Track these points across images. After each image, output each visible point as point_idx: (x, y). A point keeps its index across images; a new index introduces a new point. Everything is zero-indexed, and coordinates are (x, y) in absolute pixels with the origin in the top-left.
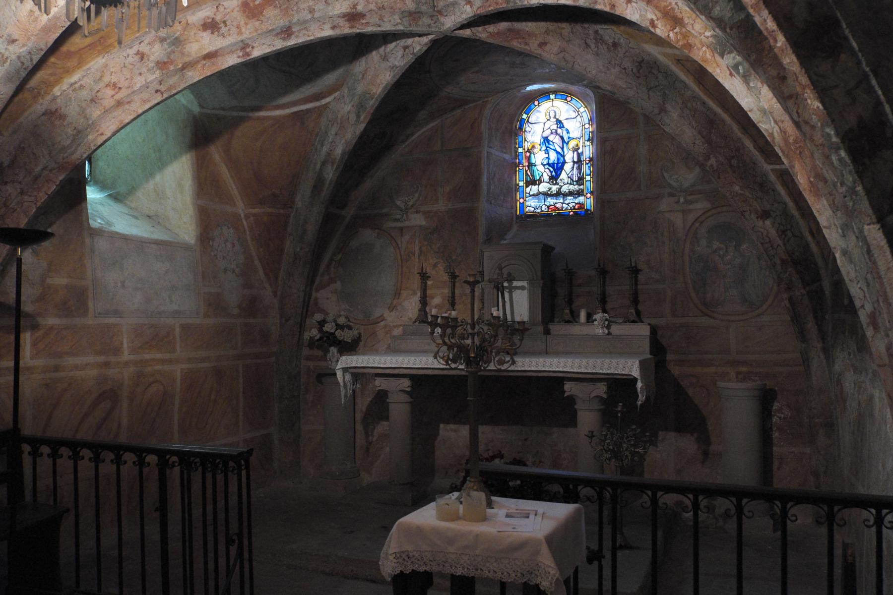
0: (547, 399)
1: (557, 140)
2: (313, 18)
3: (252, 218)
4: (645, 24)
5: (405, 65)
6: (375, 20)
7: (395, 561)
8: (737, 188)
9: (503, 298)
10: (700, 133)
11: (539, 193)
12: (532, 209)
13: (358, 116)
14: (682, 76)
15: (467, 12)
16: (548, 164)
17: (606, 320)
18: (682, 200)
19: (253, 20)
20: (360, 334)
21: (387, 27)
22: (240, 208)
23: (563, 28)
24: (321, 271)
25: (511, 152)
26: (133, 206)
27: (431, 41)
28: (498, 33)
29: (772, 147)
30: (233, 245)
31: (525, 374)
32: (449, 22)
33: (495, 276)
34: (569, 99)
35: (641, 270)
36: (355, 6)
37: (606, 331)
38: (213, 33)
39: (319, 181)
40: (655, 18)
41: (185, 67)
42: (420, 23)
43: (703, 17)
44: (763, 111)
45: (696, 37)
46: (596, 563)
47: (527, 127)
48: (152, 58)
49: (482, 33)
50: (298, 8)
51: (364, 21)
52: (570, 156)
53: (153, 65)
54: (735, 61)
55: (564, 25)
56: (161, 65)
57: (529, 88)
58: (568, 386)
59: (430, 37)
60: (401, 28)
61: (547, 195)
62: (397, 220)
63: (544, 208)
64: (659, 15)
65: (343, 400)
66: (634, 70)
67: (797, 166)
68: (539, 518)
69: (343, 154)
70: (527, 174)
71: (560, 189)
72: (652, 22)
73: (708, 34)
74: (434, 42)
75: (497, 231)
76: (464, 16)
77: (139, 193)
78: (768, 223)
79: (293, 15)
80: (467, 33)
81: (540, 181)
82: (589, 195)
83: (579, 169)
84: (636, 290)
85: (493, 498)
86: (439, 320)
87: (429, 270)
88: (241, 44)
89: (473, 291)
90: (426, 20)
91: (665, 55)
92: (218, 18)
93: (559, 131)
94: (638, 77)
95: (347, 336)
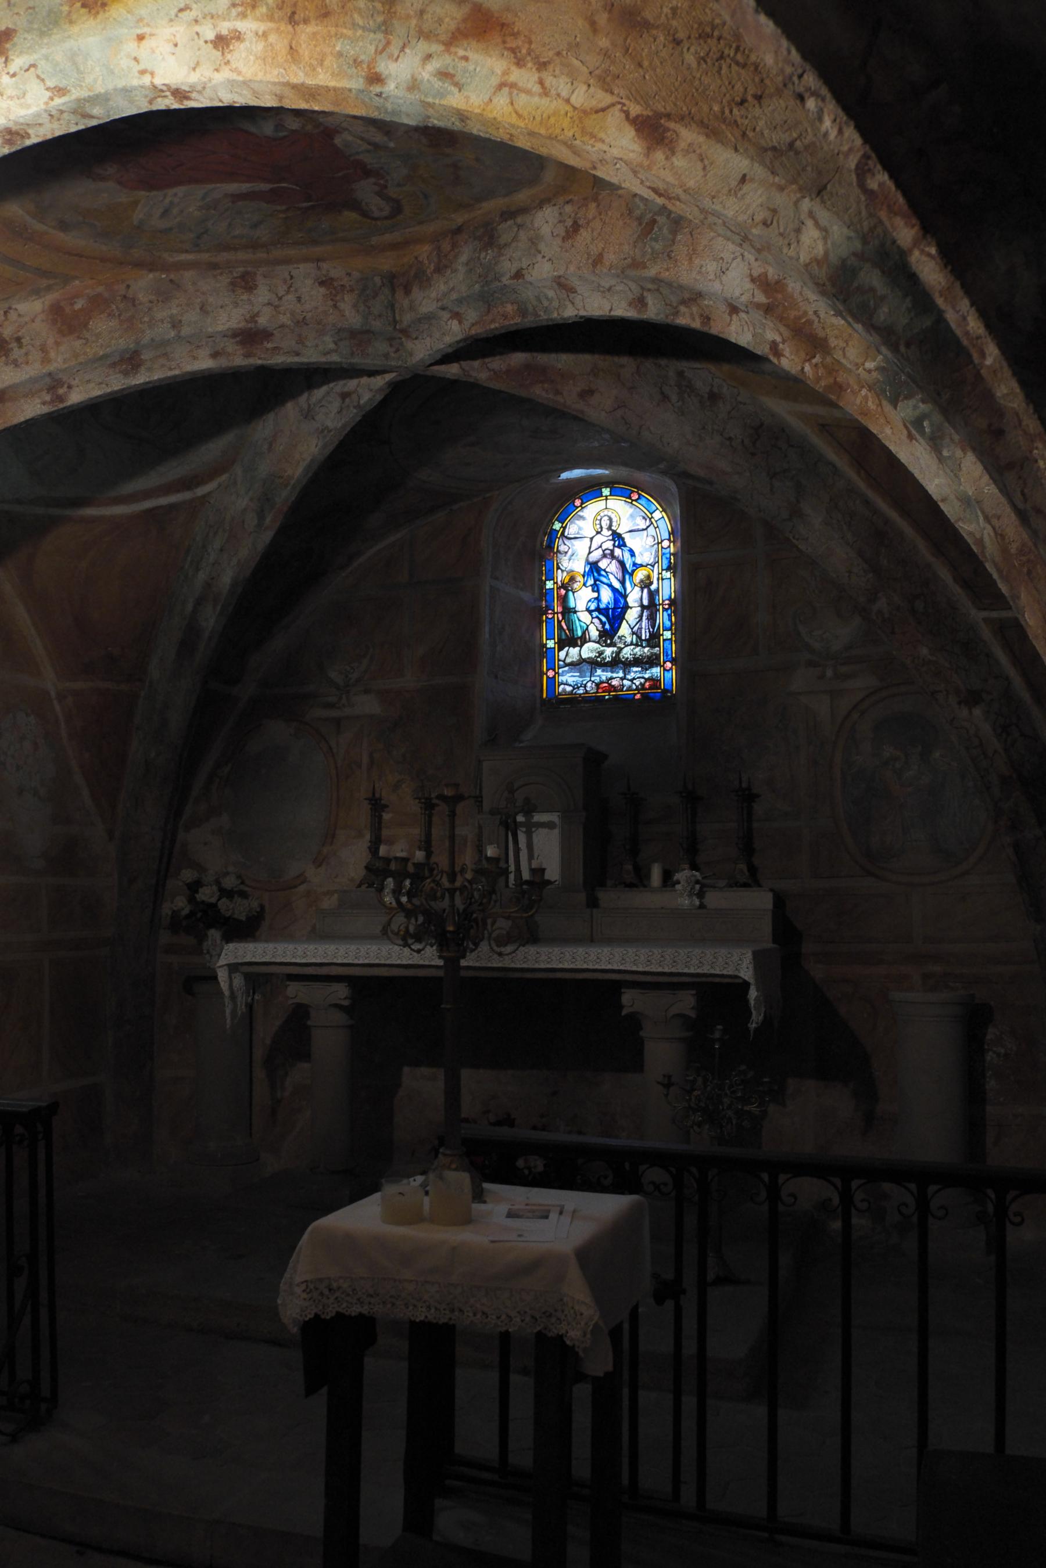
0: (589, 1019)
1: (613, 567)
2: (179, 337)
4: (762, 350)
7: (305, 1295)
8: (924, 651)
9: (516, 842)
11: (582, 661)
12: (569, 689)
13: (261, 515)
15: (454, 332)
17: (697, 882)
18: (829, 673)
20: (262, 907)
21: (311, 356)
23: (622, 366)
27: (390, 384)
29: (981, 564)
31: (551, 975)
32: (421, 350)
34: (635, 496)
35: (758, 796)
36: (253, 318)
37: (697, 902)
40: (778, 339)
43: (859, 327)
44: (966, 501)
45: (850, 371)
46: (670, 1304)
49: (479, 371)
51: (270, 345)
52: (635, 596)
54: (917, 413)
55: (624, 360)
57: (565, 475)
58: (628, 997)
59: (389, 377)
60: (335, 358)
61: (594, 664)
64: (787, 333)
65: (228, 1021)
67: (1025, 598)
68: (566, 1219)
72: (774, 346)
73: (870, 365)
74: (396, 389)
76: (448, 339)
78: (977, 712)
79: (143, 332)
80: (453, 370)
81: (584, 640)
82: (669, 665)
83: (652, 619)
85: (485, 1185)
86: (393, 866)
88: (48, 380)
89: (453, 814)
90: (381, 347)
93: (618, 552)
94: (753, 454)
95: (239, 909)
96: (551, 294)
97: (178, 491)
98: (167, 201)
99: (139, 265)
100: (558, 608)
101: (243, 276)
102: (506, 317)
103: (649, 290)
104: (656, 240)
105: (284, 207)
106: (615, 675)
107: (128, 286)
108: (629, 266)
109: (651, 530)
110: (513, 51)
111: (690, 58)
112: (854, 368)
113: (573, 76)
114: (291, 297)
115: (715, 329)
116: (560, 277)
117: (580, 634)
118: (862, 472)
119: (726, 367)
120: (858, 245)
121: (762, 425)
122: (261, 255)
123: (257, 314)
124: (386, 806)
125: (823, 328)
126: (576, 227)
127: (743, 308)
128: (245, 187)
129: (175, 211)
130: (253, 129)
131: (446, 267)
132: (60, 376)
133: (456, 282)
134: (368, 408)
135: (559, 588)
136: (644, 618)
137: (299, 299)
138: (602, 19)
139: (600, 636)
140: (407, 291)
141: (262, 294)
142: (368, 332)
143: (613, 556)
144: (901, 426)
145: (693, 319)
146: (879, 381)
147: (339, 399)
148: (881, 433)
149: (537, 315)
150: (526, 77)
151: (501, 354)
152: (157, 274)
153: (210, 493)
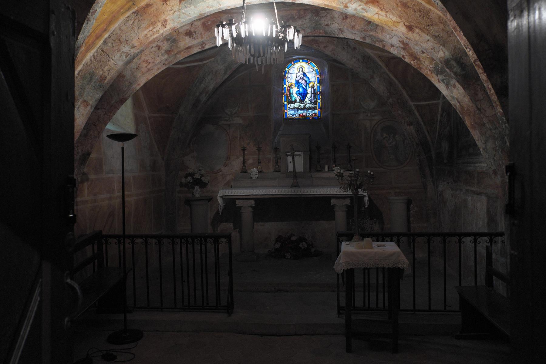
1: (303, 82)
8: (400, 112)
11: (294, 108)
18: (369, 115)
40: (405, 54)
48: (164, 48)
52: (309, 90)
53: (164, 52)
56: (168, 52)
58: (333, 201)
61: (298, 109)
62: (227, 121)
78: (412, 127)
92: (192, 30)
93: (304, 78)
110: (380, 7)
111: (418, 15)
113: (393, 14)
120: (451, 57)
138: (399, 4)
143: (303, 79)
150: (383, 13)
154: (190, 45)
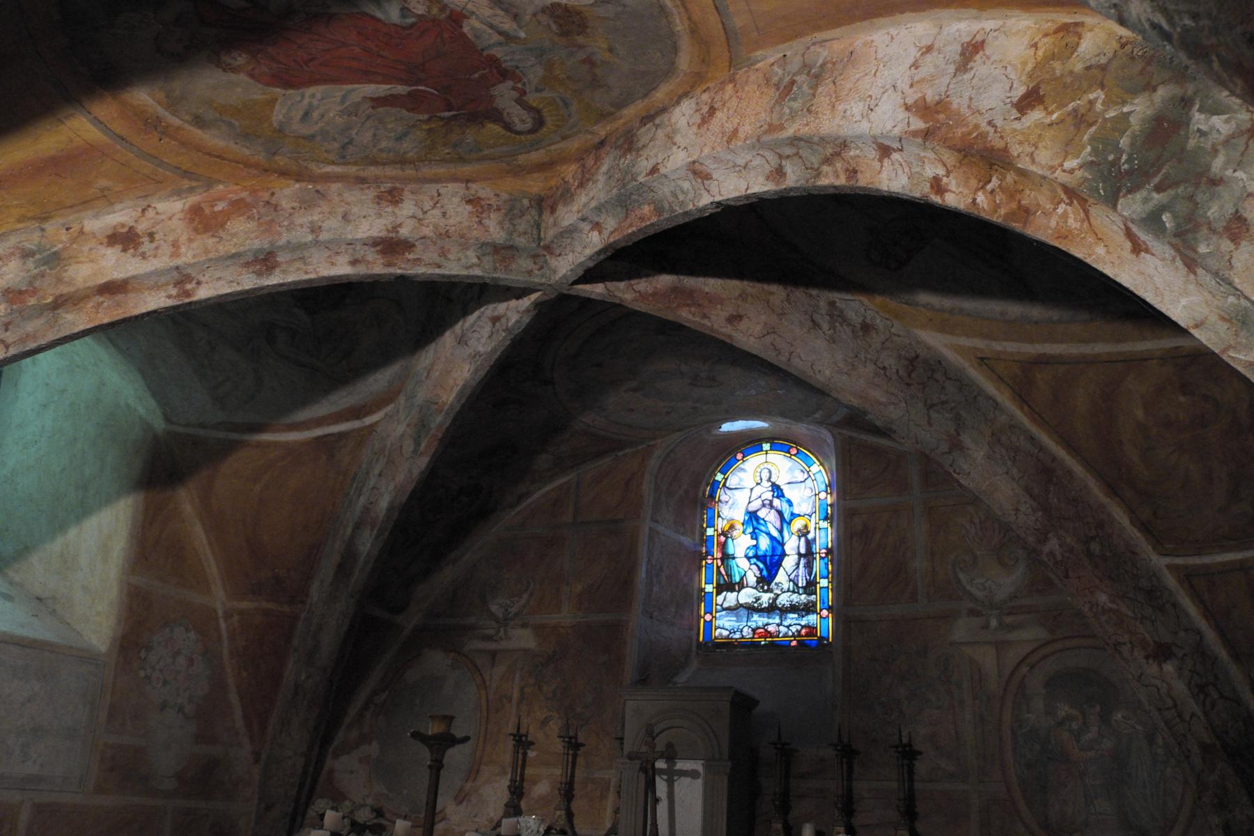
3: (236, 618)
5: (494, 350)
6: (432, 255)
8: (1103, 598)
10: (1028, 490)
11: (739, 606)
12: (725, 633)
13: (417, 443)
14: (990, 388)
15: (592, 243)
16: (756, 556)
18: (994, 623)
19: (205, 236)
22: (219, 598)
23: (772, 293)
24: (347, 720)
25: (693, 533)
26: (17, 579)
27: (537, 304)
28: (654, 294)
30: (191, 661)
33: (644, 749)
34: (794, 451)
35: (920, 753)
36: (395, 228)
38: (124, 250)
39: (349, 555)
40: (941, 171)
41: (59, 303)
42: (514, 266)
47: (722, 495)
50: (292, 223)
51: (411, 256)
52: (792, 545)
54: (1150, 206)
55: (774, 288)
57: (727, 427)
60: (477, 272)
61: (751, 609)
62: (489, 638)
63: (747, 632)
64: (950, 158)
66: (901, 372)
69: (390, 509)
70: (719, 573)
71: (775, 600)
75: (658, 669)
76: (588, 252)
77: (34, 559)
78: (1169, 667)
79: (280, 234)
81: (741, 585)
82: (825, 613)
83: (809, 566)
84: (911, 791)
87: (534, 733)
88: (175, 273)
89: (437, 767)
90: (525, 263)
91: (960, 350)
92: (141, 227)
93: (776, 502)
94: (909, 385)
96: (686, 185)
97: (347, 420)
98: (306, 102)
99: (284, 173)
100: (717, 554)
101: (390, 192)
102: (645, 218)
103: (788, 157)
104: (794, 99)
105: (426, 116)
106: (771, 621)
107: (273, 194)
108: (765, 132)
109: (809, 482)
112: (1048, 174)
114: (437, 212)
115: (863, 181)
116: (694, 162)
117: (738, 579)
118: (1026, 408)
119: (879, 299)
121: (917, 357)
122: (410, 172)
123: (400, 225)
124: (532, 743)
125: (1002, 137)
126: (712, 111)
127: (896, 145)
128: (382, 89)
129: (315, 115)
130: (379, 15)
131: (588, 180)
132: (189, 271)
133: (599, 190)
134: (516, 332)
135: (719, 535)
136: (801, 565)
137: (444, 214)
139: (758, 582)
140: (553, 210)
141: (408, 207)
142: (511, 247)
144: (1120, 238)
145: (838, 177)
146: (1086, 180)
147: (490, 324)
148: (1090, 255)
149: (673, 211)
151: (647, 276)
152: (304, 184)
153: (376, 423)
154: (118, 275)
